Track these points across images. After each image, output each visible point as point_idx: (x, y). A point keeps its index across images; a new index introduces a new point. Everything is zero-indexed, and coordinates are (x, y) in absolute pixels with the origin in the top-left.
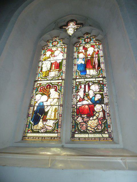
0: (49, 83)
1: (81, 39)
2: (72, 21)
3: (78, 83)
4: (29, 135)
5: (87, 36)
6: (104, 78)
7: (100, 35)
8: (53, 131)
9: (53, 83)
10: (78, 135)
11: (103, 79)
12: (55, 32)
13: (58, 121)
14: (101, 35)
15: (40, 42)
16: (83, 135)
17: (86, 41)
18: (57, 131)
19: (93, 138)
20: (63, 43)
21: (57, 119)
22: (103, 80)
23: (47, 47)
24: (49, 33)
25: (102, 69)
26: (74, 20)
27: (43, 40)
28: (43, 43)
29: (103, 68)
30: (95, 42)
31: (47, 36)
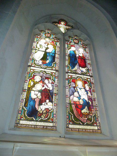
0: (43, 71)
1: (42, 32)
2: (63, 20)
3: (32, 71)
4: (21, 122)
5: (48, 31)
6: (57, 71)
7: (87, 41)
8: (92, 124)
9: (47, 72)
10: (86, 127)
11: (90, 77)
12: (49, 25)
13: (53, 110)
14: (88, 40)
15: (35, 29)
16: (41, 124)
17: (47, 35)
18: (52, 120)
19: (45, 126)
20: (55, 37)
21: (94, 113)
22: (55, 73)
23: (40, 36)
24: (44, 24)
25: (56, 63)
26: (65, 20)
27: (38, 28)
28: (37, 31)
29: (57, 63)
30: (83, 45)
31: (41, 26)
